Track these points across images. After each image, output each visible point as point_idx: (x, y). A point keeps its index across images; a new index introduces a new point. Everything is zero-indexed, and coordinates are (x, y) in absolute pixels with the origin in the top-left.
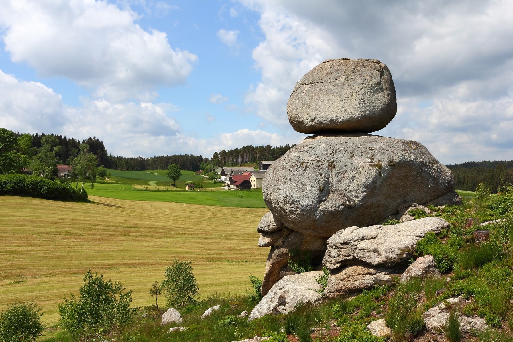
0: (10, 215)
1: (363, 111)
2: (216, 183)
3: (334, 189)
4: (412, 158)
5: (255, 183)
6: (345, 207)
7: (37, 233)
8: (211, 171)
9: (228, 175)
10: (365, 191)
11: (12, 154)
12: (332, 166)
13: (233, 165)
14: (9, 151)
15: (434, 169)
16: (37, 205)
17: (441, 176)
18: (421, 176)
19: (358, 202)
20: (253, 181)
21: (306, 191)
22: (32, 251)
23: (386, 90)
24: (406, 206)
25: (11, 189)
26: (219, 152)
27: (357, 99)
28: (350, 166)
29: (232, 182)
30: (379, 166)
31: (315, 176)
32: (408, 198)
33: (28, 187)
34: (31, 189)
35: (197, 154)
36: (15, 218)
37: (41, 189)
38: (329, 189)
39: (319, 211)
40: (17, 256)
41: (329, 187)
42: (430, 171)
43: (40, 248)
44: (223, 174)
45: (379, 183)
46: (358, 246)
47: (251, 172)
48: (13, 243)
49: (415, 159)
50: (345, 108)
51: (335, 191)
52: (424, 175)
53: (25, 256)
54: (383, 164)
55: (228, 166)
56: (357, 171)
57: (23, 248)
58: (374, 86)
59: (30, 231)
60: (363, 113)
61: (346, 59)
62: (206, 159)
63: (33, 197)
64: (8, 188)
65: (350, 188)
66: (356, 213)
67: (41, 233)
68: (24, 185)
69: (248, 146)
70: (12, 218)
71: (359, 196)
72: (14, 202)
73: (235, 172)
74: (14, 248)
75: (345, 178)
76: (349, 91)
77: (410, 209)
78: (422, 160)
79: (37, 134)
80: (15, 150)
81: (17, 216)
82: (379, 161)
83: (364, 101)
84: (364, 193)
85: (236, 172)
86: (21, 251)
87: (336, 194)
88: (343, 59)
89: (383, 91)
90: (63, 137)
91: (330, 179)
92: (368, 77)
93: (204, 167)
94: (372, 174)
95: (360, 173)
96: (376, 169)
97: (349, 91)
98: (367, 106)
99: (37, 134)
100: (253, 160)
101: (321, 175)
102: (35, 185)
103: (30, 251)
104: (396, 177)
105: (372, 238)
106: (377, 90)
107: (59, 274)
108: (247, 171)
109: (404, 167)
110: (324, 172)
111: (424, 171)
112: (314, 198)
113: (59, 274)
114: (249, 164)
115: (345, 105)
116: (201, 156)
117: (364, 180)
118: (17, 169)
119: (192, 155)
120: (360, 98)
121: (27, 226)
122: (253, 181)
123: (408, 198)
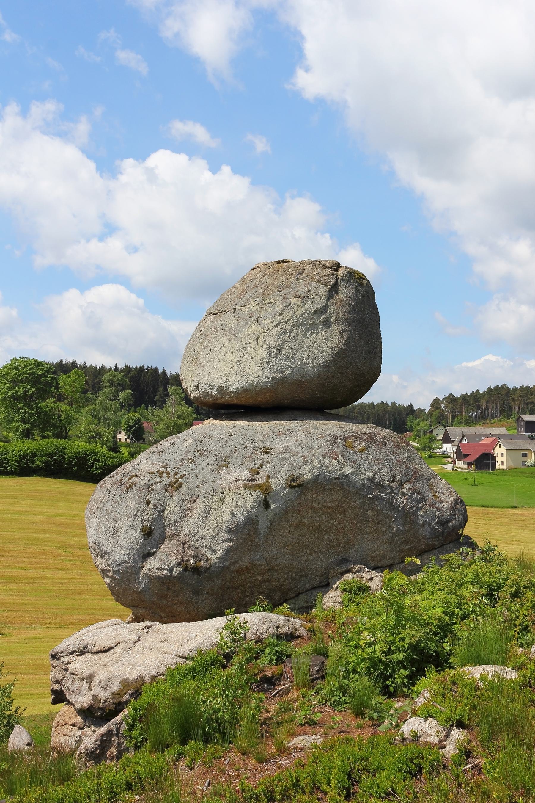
0: (30, 513)
1: (277, 371)
2: (430, 456)
3: (173, 532)
4: (347, 470)
5: (504, 459)
6: (186, 569)
7: (64, 547)
8: (425, 433)
9: (456, 443)
10: (230, 540)
11: (47, 404)
12: (175, 486)
13: (469, 422)
14: (44, 399)
15: (403, 494)
16: (80, 495)
17: (422, 508)
18: (372, 509)
19: (216, 561)
20: (500, 455)
21: (118, 534)
22: (45, 578)
23: (337, 322)
24: (340, 571)
25: (42, 465)
26: (441, 398)
27: (265, 347)
28: (208, 487)
29: (461, 455)
30: (266, 490)
31: (137, 506)
32: (352, 552)
33: (70, 462)
34: (74, 466)
35: (403, 401)
36: (36, 518)
37: (92, 467)
38: (164, 532)
39: (141, 575)
40: (15, 587)
41: (164, 527)
42: (393, 498)
43: (61, 574)
44: (447, 439)
45: (263, 524)
46: (70, 666)
47: (499, 437)
48: (18, 562)
49: (353, 473)
50: (243, 365)
51: (173, 536)
52: (378, 506)
53: (28, 587)
54: (274, 483)
55: (459, 424)
56: (217, 498)
57: (31, 573)
58: (307, 319)
59: (53, 542)
60: (276, 374)
61: (283, 261)
62: (421, 411)
63: (78, 480)
64: (38, 463)
65: (201, 532)
66: (218, 582)
67: (72, 546)
68: (64, 458)
69: (497, 387)
70: (31, 517)
71: (218, 548)
72: (42, 488)
73: (469, 436)
74: (16, 572)
75: (194, 512)
76: (254, 329)
77: (348, 577)
78: (371, 475)
79: (116, 366)
80: (54, 397)
81: (41, 513)
82: (269, 476)
83: (280, 350)
84: (227, 544)
85: (470, 437)
86: (26, 578)
87: (173, 542)
88: (278, 262)
89: (329, 327)
90: (160, 371)
91: (166, 512)
92: (296, 301)
93: (414, 426)
94: (247, 504)
95: (222, 501)
96: (256, 494)
97: (254, 329)
98: (288, 358)
99: (116, 366)
100: (508, 412)
101: (148, 503)
102: (84, 458)
103: (41, 578)
104: (312, 508)
105: (100, 652)
106: (314, 326)
107: (72, 624)
108: (492, 435)
109: (330, 490)
110: (154, 499)
111: (378, 498)
112: (132, 548)
113: (72, 624)
114: (501, 420)
115: (243, 359)
116: (411, 405)
117: (227, 516)
118: (57, 431)
119: (394, 404)
120: (272, 345)
121: (52, 533)
122: (500, 455)
123: (352, 552)
